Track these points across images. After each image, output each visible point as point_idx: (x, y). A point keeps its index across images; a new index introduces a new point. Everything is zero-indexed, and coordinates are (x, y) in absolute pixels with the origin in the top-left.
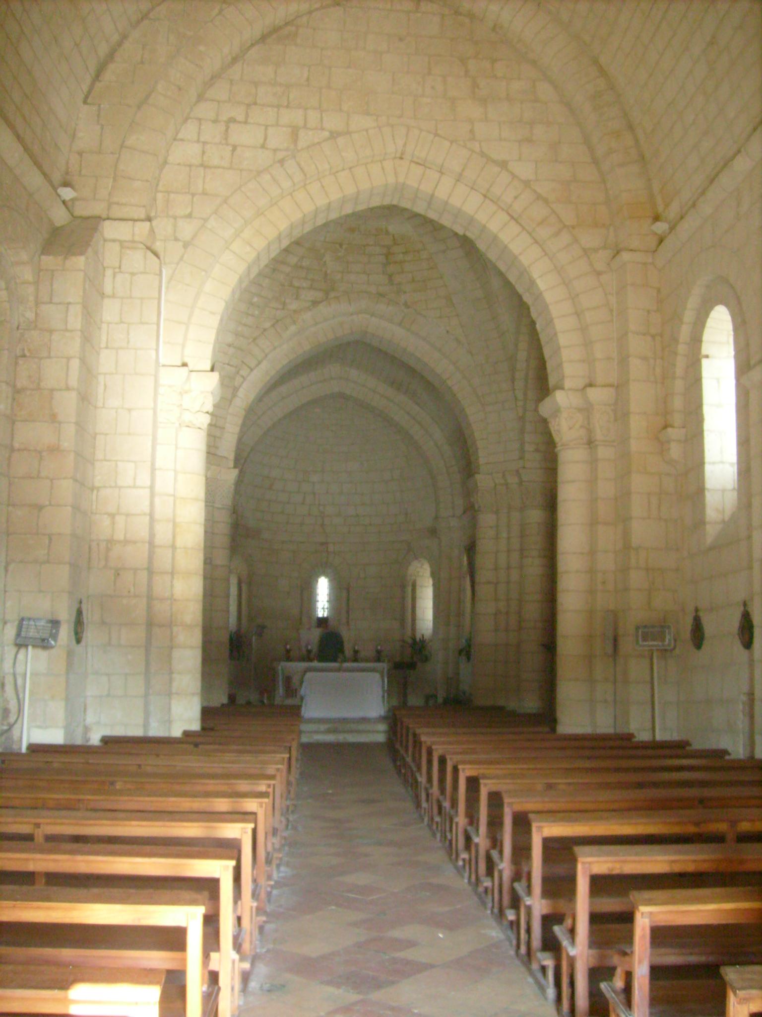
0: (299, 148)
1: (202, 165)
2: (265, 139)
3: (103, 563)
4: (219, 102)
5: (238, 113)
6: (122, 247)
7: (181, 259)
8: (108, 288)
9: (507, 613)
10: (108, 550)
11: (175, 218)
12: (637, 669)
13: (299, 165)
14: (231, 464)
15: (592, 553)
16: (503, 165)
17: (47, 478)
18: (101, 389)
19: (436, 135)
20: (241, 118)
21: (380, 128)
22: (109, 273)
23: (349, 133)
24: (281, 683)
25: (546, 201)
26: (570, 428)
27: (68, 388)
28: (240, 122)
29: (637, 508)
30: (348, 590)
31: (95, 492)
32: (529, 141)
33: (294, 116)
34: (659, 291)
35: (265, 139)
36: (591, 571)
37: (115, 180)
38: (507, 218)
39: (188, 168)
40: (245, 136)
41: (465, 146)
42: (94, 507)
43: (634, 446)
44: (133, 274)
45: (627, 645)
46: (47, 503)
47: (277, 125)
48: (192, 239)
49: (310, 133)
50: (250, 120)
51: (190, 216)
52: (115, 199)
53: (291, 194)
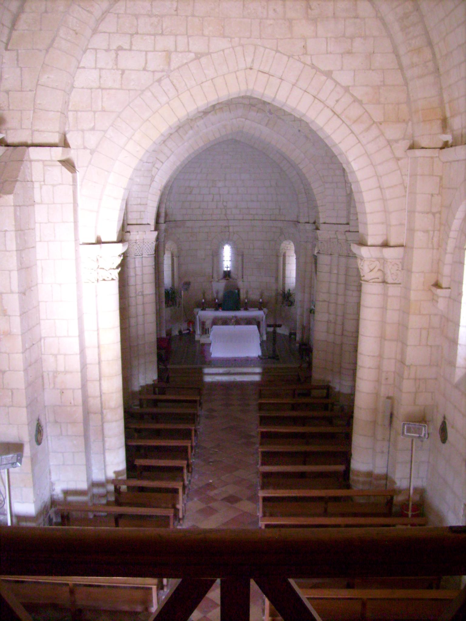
0: (172, 69)
1: (100, 88)
2: (146, 63)
3: (52, 386)
4: (109, 33)
5: (124, 42)
6: (44, 166)
7: (90, 163)
8: (37, 198)
9: (335, 323)
10: (55, 377)
11: (83, 131)
12: (403, 442)
13: (172, 83)
14: (153, 228)
15: (380, 356)
16: (329, 74)
17: (5, 353)
18: (39, 270)
19: (277, 51)
20: (127, 47)
21: (233, 48)
22: (37, 185)
23: (209, 53)
24: (198, 327)
25: (360, 102)
26: (371, 271)
27: (12, 292)
28: (125, 50)
29: (412, 338)
30: (243, 255)
31: (42, 341)
32: (349, 53)
33: (167, 42)
34: (441, 178)
35: (146, 63)
36: (379, 368)
37: (34, 112)
38: (331, 114)
39: (89, 91)
40: (130, 61)
41: (299, 60)
42: (43, 350)
43: (413, 296)
44: (54, 186)
45: (398, 424)
46: (8, 369)
47: (154, 51)
48: (97, 147)
49: (180, 55)
50: (134, 48)
51: (93, 129)
52: (36, 128)
53: (168, 103)
